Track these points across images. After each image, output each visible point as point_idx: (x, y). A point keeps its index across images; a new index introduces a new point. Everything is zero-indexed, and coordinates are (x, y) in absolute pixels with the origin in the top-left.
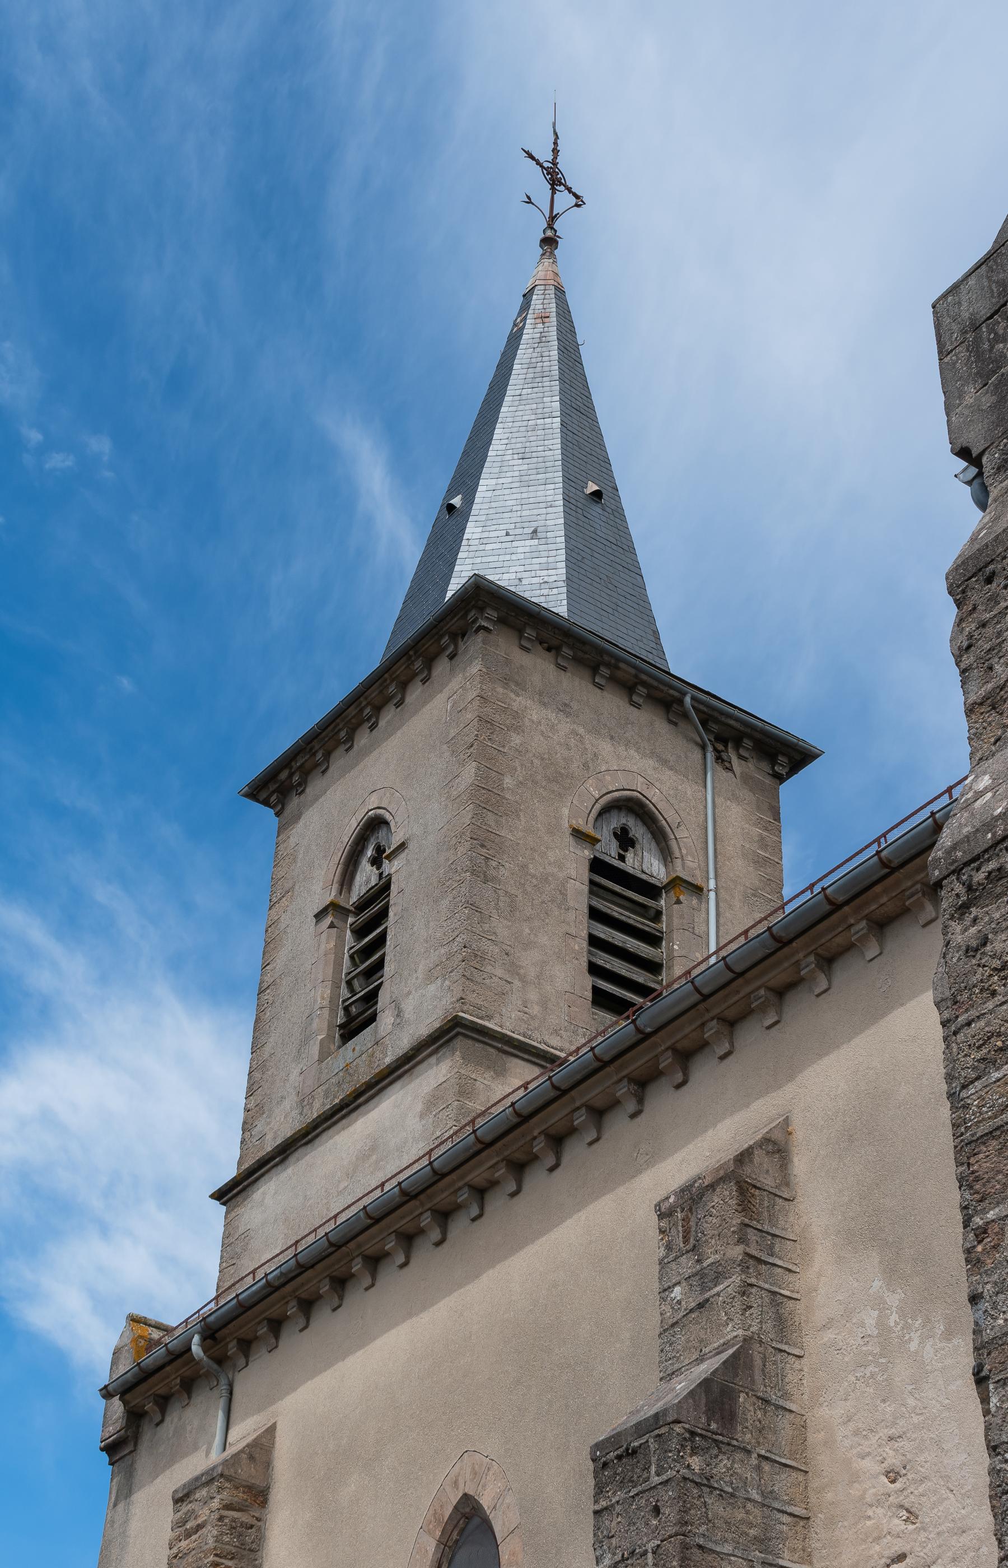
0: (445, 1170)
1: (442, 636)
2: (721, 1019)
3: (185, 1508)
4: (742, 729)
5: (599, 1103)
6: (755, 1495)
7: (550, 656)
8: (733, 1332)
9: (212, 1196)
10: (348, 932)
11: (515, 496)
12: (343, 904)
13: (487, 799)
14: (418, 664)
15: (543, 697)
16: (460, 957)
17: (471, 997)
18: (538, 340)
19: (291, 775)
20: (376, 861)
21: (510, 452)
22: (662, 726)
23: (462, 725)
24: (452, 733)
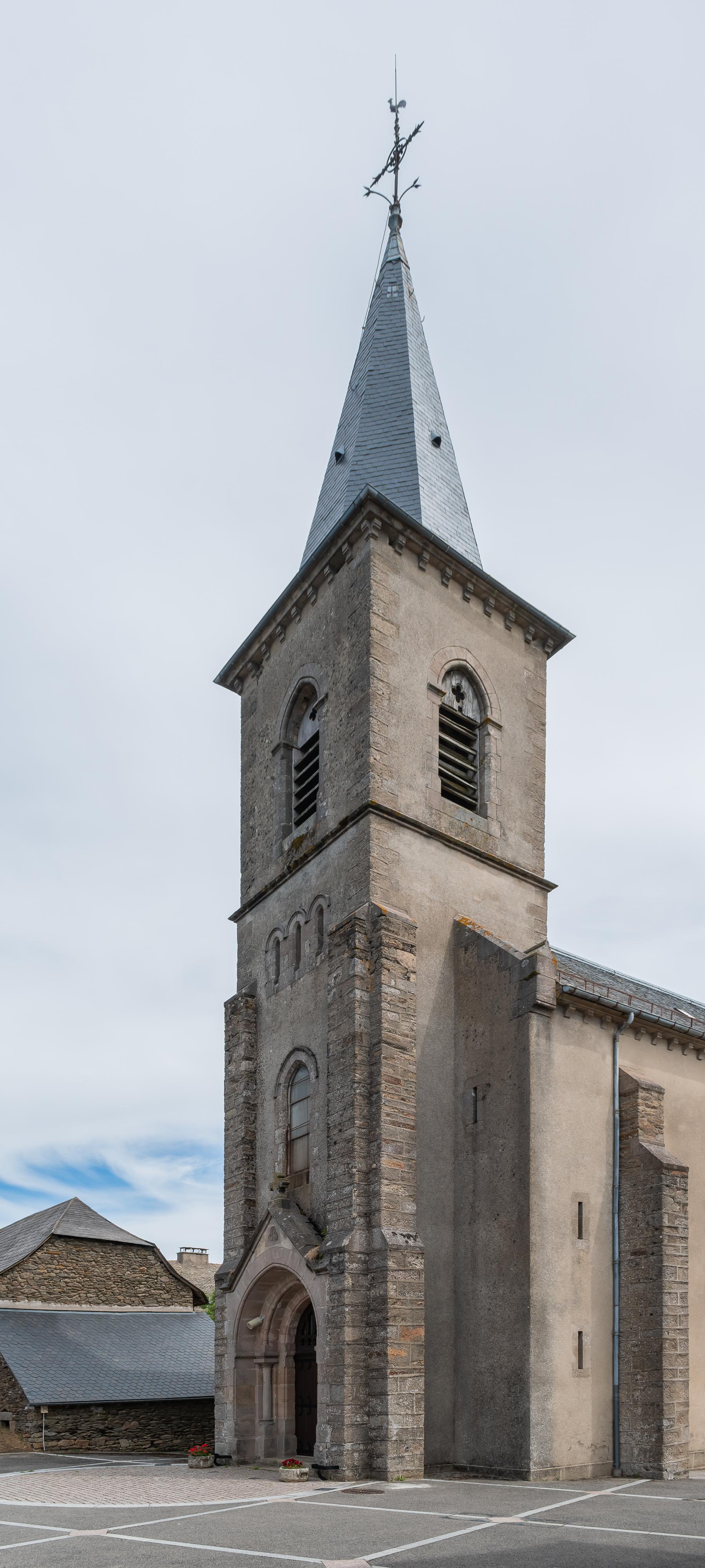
9: (230, 919)
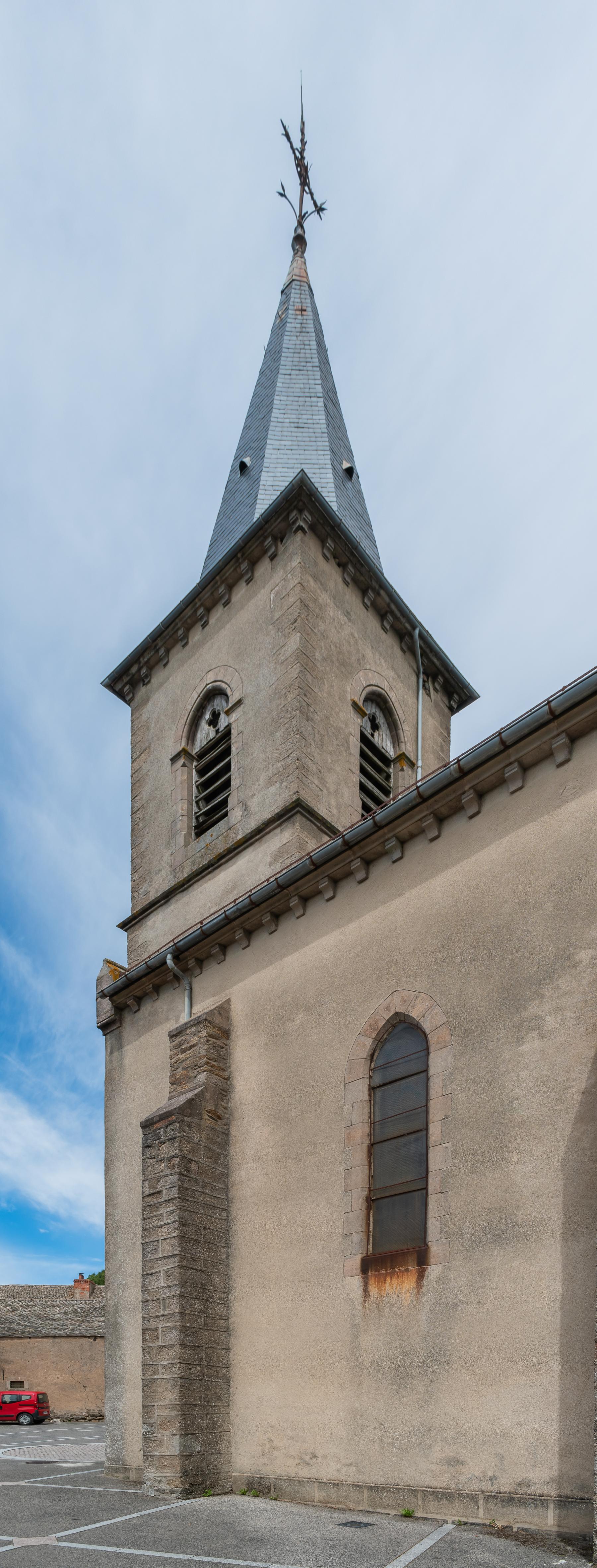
0: (384, 823)
1: (266, 538)
3: (178, 1040)
4: (440, 667)
9: (118, 926)
10: (194, 772)
12: (190, 751)
14: (244, 566)
16: (295, 766)
18: (299, 330)
19: (140, 669)
21: (287, 420)
23: (286, 608)
24: (277, 615)
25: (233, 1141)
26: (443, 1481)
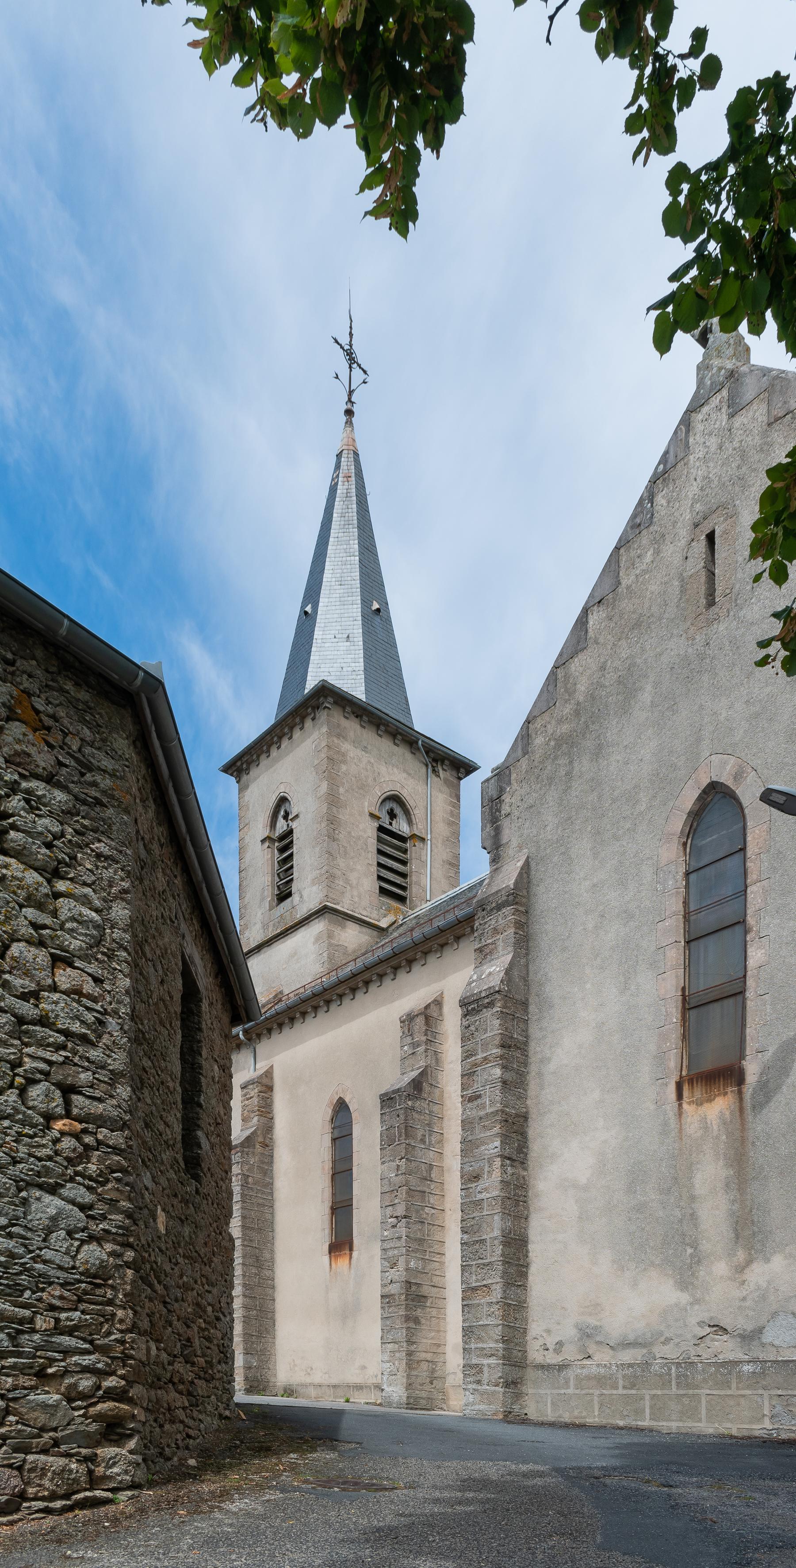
1: (308, 708)
2: (422, 952)
3: (245, 1091)
5: (381, 973)
6: (427, 1112)
7: (357, 720)
8: (422, 1063)
11: (338, 611)
13: (333, 800)
14: (298, 720)
15: (356, 743)
17: (330, 895)
19: (242, 764)
20: (286, 817)
22: (408, 755)
25: (275, 1160)
26: (358, 1380)
